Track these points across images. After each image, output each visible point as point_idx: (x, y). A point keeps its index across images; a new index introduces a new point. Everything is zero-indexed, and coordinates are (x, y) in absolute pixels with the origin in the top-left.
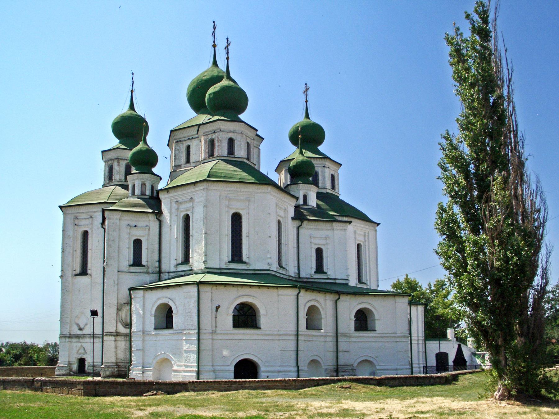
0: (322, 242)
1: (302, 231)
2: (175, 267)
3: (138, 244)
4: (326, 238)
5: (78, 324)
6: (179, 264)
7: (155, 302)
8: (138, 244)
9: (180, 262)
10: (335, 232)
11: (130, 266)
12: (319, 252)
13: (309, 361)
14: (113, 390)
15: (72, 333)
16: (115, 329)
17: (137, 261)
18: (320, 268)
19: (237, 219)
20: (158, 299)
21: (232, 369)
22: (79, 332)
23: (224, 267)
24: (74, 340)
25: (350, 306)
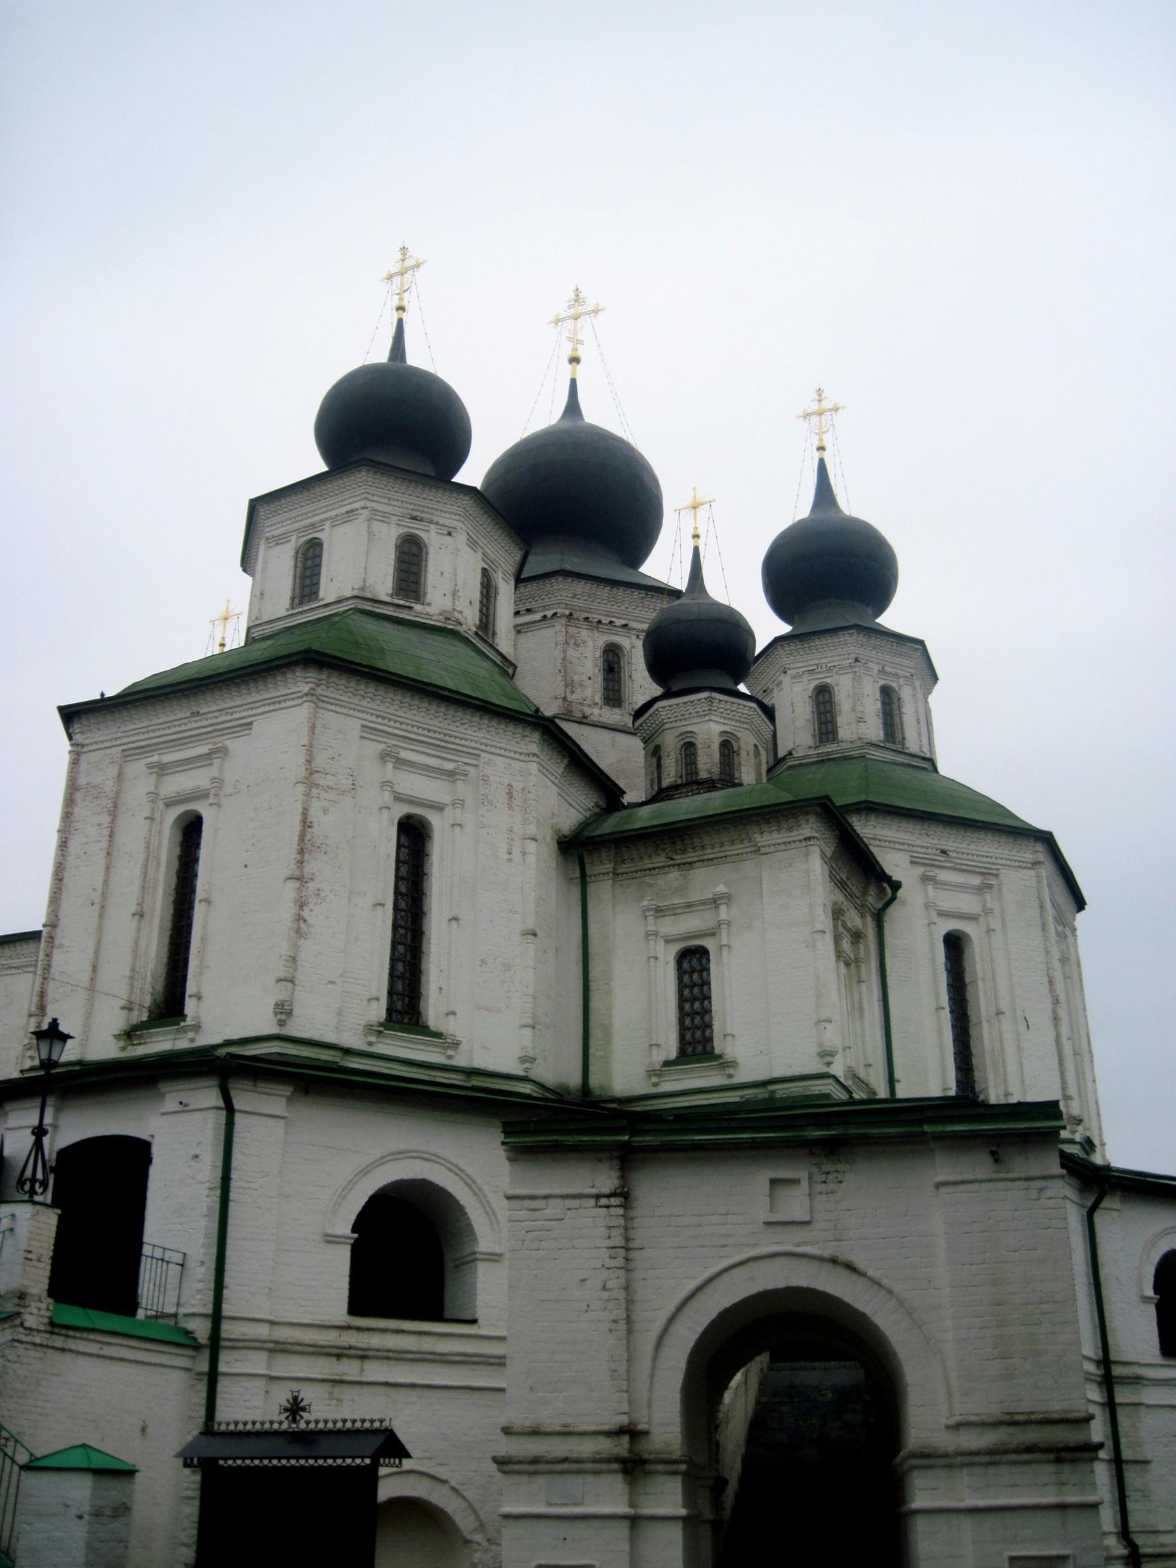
6: (667, 1064)
19: (413, 836)
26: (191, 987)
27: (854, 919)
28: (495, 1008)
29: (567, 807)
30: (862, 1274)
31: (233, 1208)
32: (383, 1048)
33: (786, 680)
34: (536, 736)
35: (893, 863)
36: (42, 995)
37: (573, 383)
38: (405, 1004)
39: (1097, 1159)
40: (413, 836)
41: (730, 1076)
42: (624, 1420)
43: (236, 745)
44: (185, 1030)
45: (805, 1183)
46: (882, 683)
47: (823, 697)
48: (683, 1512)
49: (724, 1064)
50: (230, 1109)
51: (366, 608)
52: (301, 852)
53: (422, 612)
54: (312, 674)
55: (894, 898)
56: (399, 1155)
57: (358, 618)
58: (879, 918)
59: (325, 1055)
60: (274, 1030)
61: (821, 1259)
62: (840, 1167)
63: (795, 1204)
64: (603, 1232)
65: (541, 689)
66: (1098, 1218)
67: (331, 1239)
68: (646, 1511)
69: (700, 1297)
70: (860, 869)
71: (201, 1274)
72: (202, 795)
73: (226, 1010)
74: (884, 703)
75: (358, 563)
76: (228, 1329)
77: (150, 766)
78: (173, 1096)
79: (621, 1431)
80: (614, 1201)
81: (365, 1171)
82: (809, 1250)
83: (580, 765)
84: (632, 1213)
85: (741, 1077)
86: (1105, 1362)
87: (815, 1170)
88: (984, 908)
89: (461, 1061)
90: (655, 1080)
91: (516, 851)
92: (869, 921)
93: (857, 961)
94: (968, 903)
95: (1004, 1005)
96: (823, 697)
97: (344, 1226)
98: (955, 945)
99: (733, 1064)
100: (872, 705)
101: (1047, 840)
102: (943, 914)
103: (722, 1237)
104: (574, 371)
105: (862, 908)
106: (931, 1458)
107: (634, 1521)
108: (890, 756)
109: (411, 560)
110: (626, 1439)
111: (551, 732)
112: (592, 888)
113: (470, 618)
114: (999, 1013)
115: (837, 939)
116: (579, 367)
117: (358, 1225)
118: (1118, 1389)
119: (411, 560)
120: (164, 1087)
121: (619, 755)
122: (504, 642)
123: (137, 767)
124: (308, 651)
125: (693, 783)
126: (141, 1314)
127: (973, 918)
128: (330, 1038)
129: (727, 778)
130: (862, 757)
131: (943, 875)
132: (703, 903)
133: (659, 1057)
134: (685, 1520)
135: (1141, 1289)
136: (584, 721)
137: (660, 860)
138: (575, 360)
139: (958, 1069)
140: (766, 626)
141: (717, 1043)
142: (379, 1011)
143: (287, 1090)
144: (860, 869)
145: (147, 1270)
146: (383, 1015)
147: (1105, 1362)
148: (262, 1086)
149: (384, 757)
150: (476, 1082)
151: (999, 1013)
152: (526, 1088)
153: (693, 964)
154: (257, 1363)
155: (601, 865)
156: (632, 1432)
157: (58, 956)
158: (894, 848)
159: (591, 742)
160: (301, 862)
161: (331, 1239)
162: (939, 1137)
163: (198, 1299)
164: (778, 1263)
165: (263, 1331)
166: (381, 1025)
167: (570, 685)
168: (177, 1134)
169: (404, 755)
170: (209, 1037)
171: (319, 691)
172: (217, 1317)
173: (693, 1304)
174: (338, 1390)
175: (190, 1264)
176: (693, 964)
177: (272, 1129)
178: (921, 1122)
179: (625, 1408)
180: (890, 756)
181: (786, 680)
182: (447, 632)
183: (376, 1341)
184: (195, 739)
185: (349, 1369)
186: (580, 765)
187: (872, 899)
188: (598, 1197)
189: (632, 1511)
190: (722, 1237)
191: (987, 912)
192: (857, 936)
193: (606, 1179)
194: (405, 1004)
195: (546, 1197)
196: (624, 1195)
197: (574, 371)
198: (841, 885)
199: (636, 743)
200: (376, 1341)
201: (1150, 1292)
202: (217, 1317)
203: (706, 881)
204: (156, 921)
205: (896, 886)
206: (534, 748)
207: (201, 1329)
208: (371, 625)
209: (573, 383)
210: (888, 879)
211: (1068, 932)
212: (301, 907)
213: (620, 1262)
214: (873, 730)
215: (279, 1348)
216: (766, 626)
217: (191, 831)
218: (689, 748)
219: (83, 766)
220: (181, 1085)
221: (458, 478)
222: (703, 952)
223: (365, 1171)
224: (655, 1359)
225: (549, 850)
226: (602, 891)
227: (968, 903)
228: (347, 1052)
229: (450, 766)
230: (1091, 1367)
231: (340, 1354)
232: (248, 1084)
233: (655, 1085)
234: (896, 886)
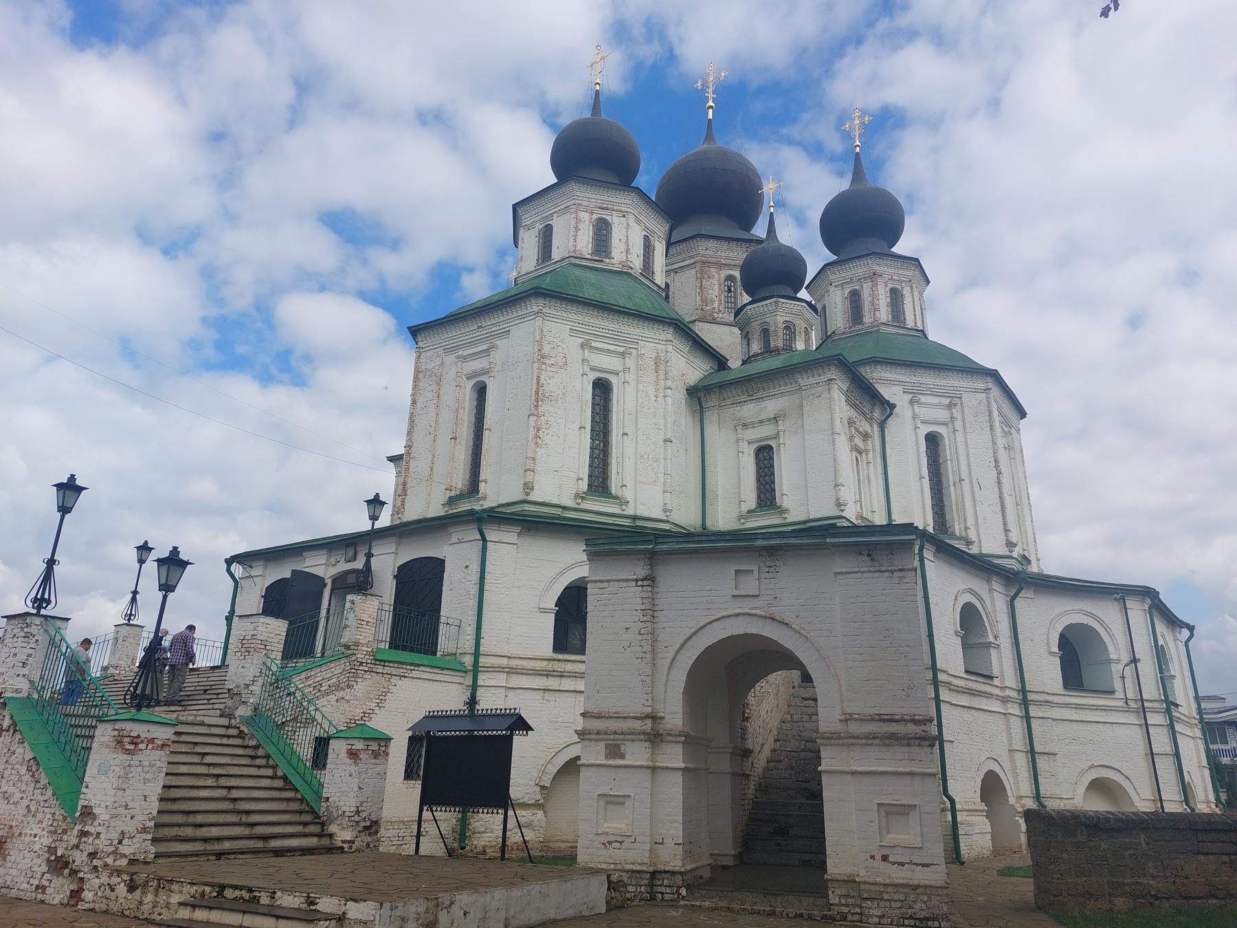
6: (749, 512)
19: (602, 389)
23: (570, 503)
25: (1044, 621)
26: (482, 477)
27: (865, 426)
28: (652, 486)
29: (693, 370)
31: (486, 595)
32: (586, 505)
33: (832, 289)
34: (671, 330)
35: (886, 392)
36: (404, 484)
38: (599, 481)
39: (1034, 568)
40: (602, 389)
42: (649, 710)
43: (501, 343)
44: (479, 500)
45: (756, 572)
46: (890, 286)
47: (855, 300)
48: (683, 765)
50: (484, 539)
51: (573, 260)
52: (537, 400)
53: (606, 264)
54: (541, 302)
55: (891, 414)
56: (1067, 612)
57: (572, 268)
58: (882, 425)
59: (558, 511)
60: (522, 497)
61: (765, 617)
62: (778, 563)
63: (750, 585)
64: (639, 601)
65: (684, 305)
66: (1017, 602)
67: (543, 611)
68: (658, 764)
69: (694, 638)
70: (867, 397)
71: (470, 630)
72: (486, 372)
73: (498, 489)
75: (573, 237)
76: (483, 660)
77: (457, 357)
78: (456, 534)
79: (647, 717)
80: (645, 583)
81: (562, 573)
82: (758, 612)
83: (700, 346)
84: (656, 590)
85: (791, 518)
86: (1023, 690)
87: (762, 565)
88: (952, 418)
89: (630, 511)
91: (661, 395)
92: (875, 427)
93: (866, 451)
94: (943, 415)
95: (964, 475)
96: (855, 300)
97: (551, 602)
98: (933, 441)
99: (785, 511)
100: (883, 300)
101: (994, 375)
103: (707, 607)
105: (870, 420)
106: (833, 738)
107: (654, 769)
108: (896, 330)
109: (602, 232)
110: (649, 722)
111: (683, 330)
112: (707, 415)
113: (637, 264)
114: (961, 480)
115: (851, 438)
117: (560, 602)
118: (1031, 708)
119: (602, 232)
120: (451, 530)
121: (725, 339)
122: (660, 279)
123: (450, 359)
124: (537, 288)
125: (768, 351)
126: (439, 654)
128: (555, 501)
129: (789, 348)
130: (878, 331)
131: (923, 399)
132: (769, 420)
133: (745, 508)
134: (684, 770)
135: (1049, 647)
136: (714, 321)
137: (744, 398)
139: (935, 514)
140: (816, 257)
142: (584, 486)
143: (518, 529)
144: (867, 397)
145: (442, 630)
146: (586, 487)
147: (1023, 690)
148: (503, 527)
149: (583, 346)
150: (639, 523)
151: (961, 480)
152: (667, 527)
153: (765, 457)
154: (500, 679)
155: (712, 401)
156: (654, 718)
157: (412, 463)
158: (890, 384)
159: (707, 332)
160: (537, 406)
161: (543, 611)
162: (835, 545)
163: (468, 644)
164: (740, 619)
165: (504, 662)
167: (705, 301)
168: (457, 555)
169: (594, 344)
170: (487, 504)
171: (545, 310)
172: (477, 654)
173: (690, 642)
174: (547, 695)
175: (463, 626)
176: (765, 457)
177: (506, 549)
178: (825, 537)
179: (650, 703)
180: (896, 330)
181: (832, 289)
182: (624, 273)
183: (569, 667)
184: (481, 341)
185: (553, 683)
186: (700, 346)
187: (877, 414)
188: (637, 581)
189: (651, 764)
190: (707, 607)
191: (626, 370)
192: (866, 436)
193: (640, 571)
194: (599, 481)
195: (608, 581)
196: (651, 579)
198: (854, 406)
199: (736, 330)
200: (569, 667)
202: (477, 654)
203: (771, 406)
204: (464, 442)
205: (893, 407)
206: (670, 337)
207: (468, 660)
208: (578, 272)
210: (888, 402)
211: (1013, 431)
212: (538, 430)
213: (648, 618)
214: (884, 315)
215: (511, 671)
216: (816, 257)
217: (481, 391)
218: (766, 333)
219: (423, 359)
220: (458, 528)
221: (897, 249)
223: (562, 573)
224: (668, 675)
225: (681, 395)
226: (711, 418)
227: (943, 415)
228: (564, 508)
229: (485, 347)
230: (1014, 694)
231: (548, 674)
232: (496, 527)
234: (893, 407)
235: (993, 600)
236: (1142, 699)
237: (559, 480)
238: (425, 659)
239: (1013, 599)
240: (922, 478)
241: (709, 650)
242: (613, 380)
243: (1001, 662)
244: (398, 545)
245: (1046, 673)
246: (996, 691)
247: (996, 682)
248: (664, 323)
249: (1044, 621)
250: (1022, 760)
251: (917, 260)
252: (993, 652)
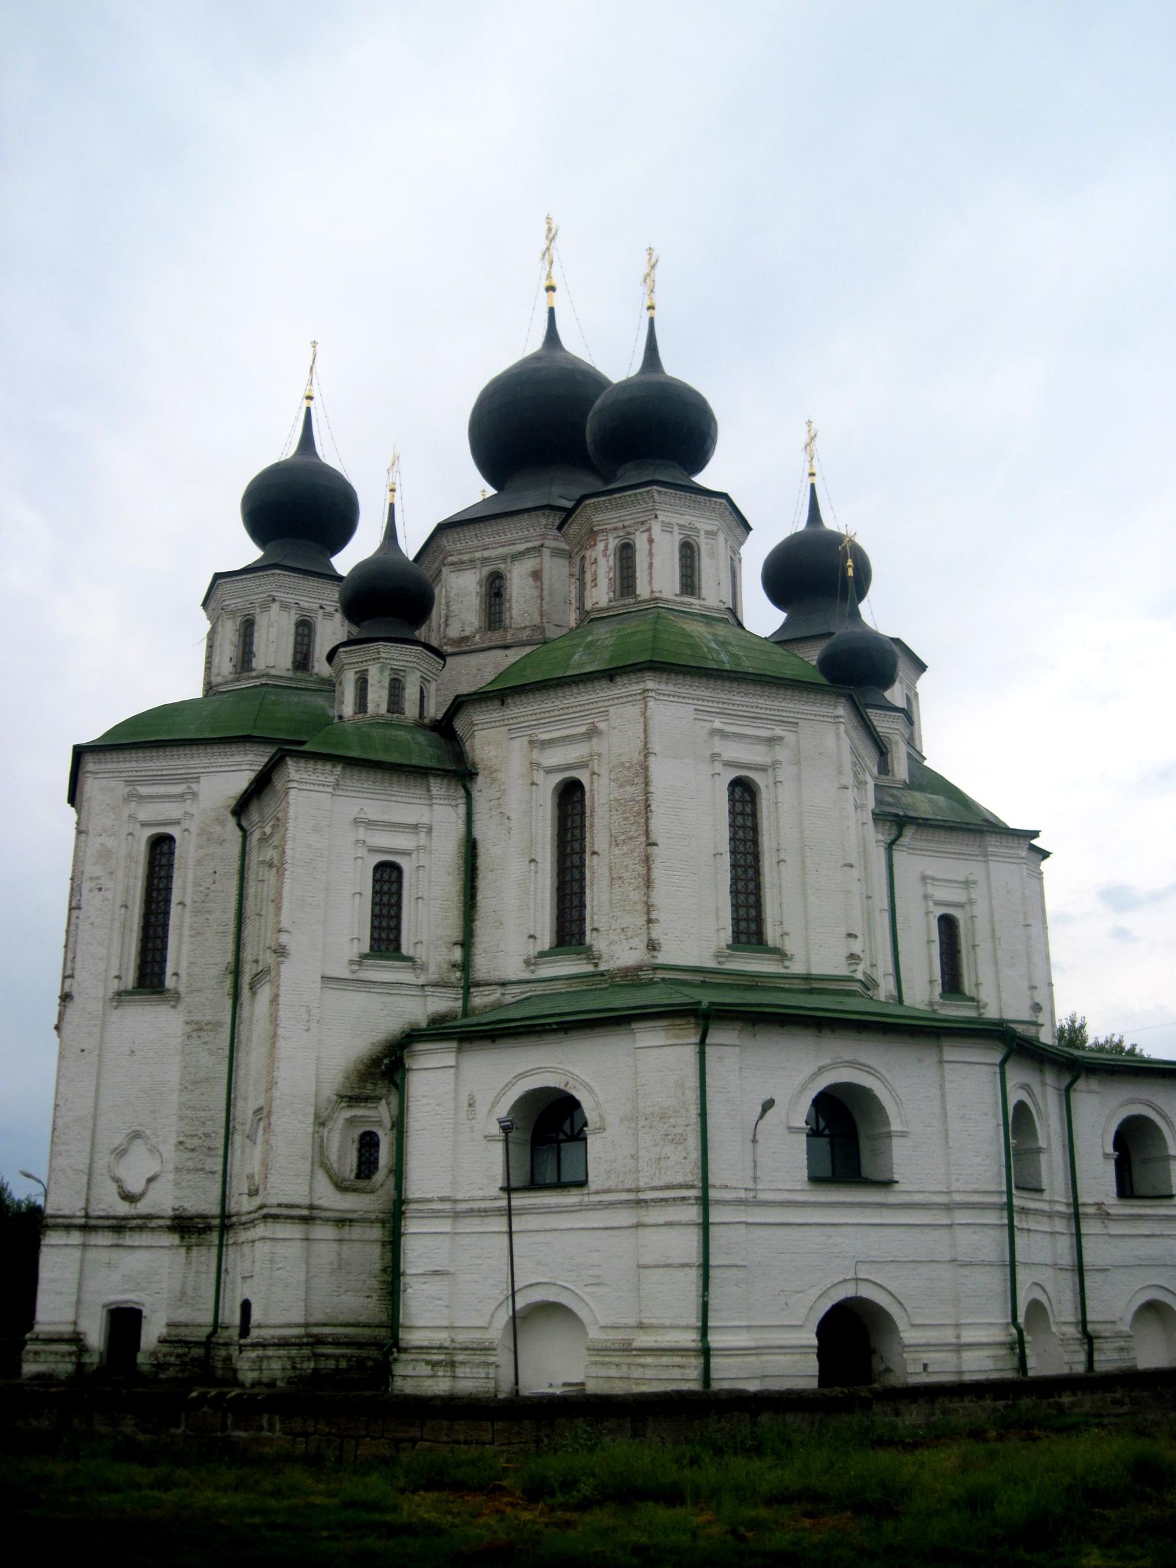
0: (957, 895)
1: (899, 857)
2: (527, 963)
3: (388, 879)
4: (967, 884)
5: (117, 1180)
6: (542, 955)
7: (510, 1085)
8: (388, 879)
9: (547, 948)
10: (992, 864)
11: (121, 996)
12: (948, 926)
13: (1134, 1307)
14: (622, 1452)
15: (97, 1210)
16: (82, 1204)
17: (385, 938)
18: (952, 981)
19: (743, 792)
20: (522, 1076)
21: (810, 1338)
22: (123, 1208)
23: (711, 964)
24: (103, 1239)
25: (1100, 1113)
30: (761, 1117)
37: (551, 311)
38: (749, 928)
40: (743, 792)
41: (786, 968)
49: (588, 953)
74: (252, 635)
90: (355, 967)
102: (144, 824)
104: (550, 299)
116: (555, 295)
127: (176, 822)
133: (533, 949)
138: (551, 289)
141: (588, 938)
166: (728, 947)
194: (749, 928)
197: (550, 299)
201: (1110, 1149)
209: (551, 311)
222: (396, 868)
233: (533, 972)
235: (1042, 1094)
236: (706, 1352)
237: (691, 931)
238: (571, 1198)
239: (1068, 1089)
240: (930, 942)
241: (1030, 1111)
242: (583, 776)
243: (1051, 1169)
244: (459, 1051)
245: (1099, 1178)
246: (1046, 1207)
247: (1046, 1196)
248: (641, 670)
249: (1100, 1113)
250: (1068, 1281)
251: (218, 576)
252: (1043, 1158)
